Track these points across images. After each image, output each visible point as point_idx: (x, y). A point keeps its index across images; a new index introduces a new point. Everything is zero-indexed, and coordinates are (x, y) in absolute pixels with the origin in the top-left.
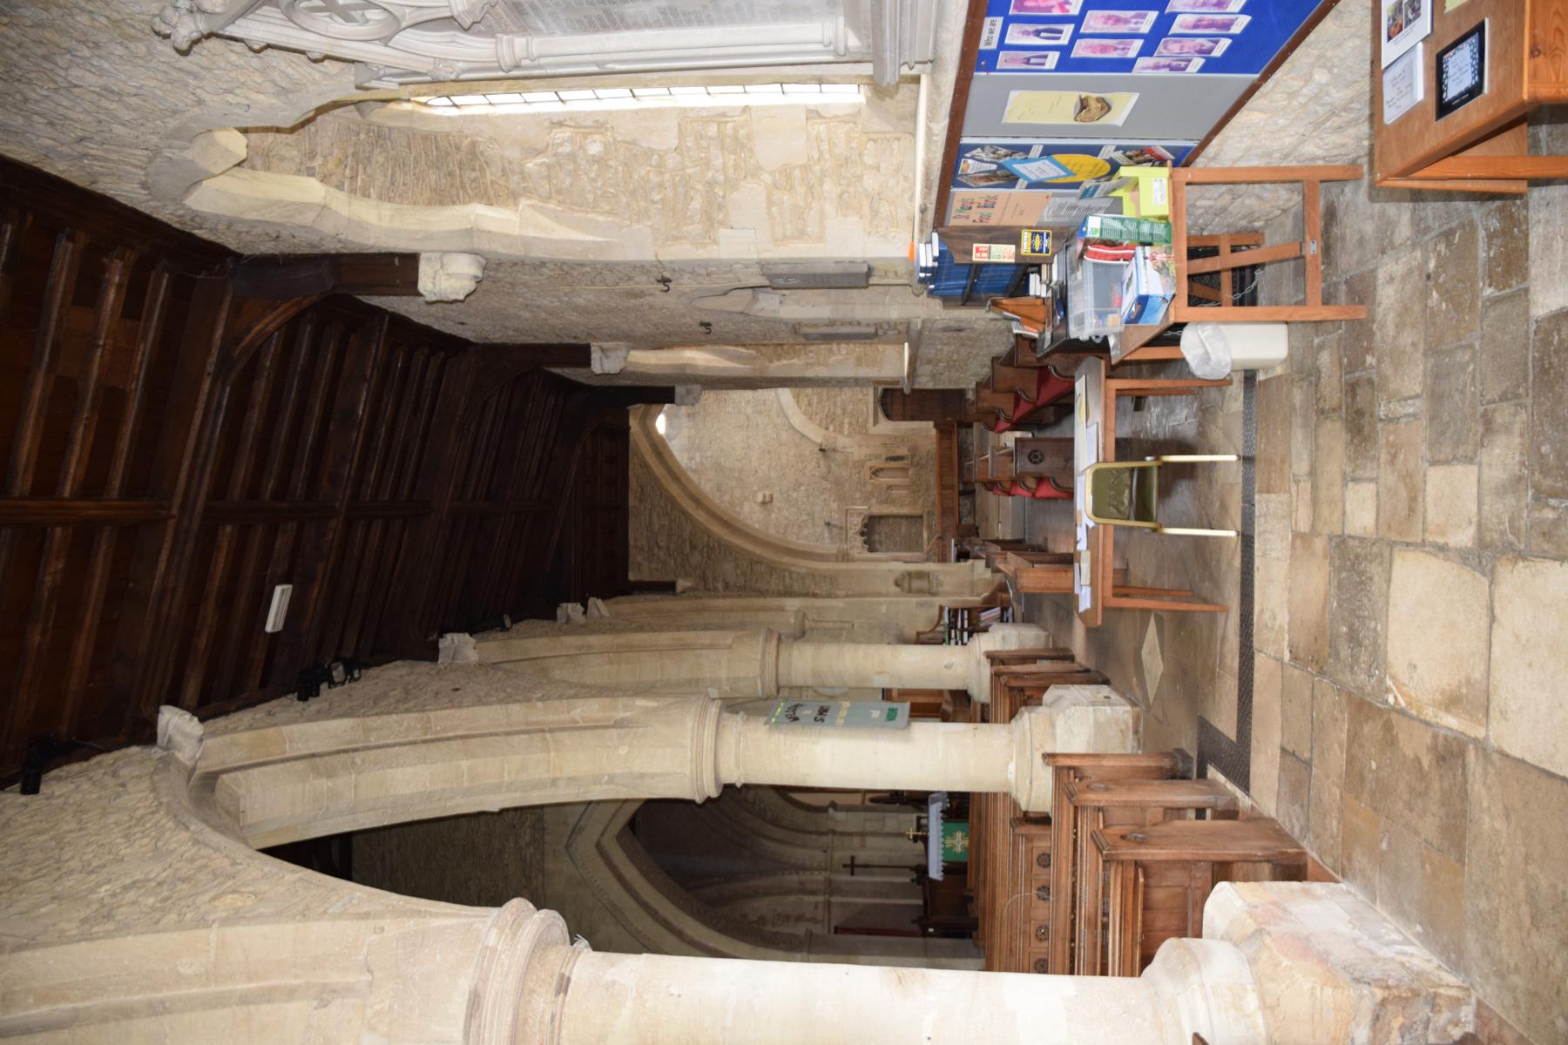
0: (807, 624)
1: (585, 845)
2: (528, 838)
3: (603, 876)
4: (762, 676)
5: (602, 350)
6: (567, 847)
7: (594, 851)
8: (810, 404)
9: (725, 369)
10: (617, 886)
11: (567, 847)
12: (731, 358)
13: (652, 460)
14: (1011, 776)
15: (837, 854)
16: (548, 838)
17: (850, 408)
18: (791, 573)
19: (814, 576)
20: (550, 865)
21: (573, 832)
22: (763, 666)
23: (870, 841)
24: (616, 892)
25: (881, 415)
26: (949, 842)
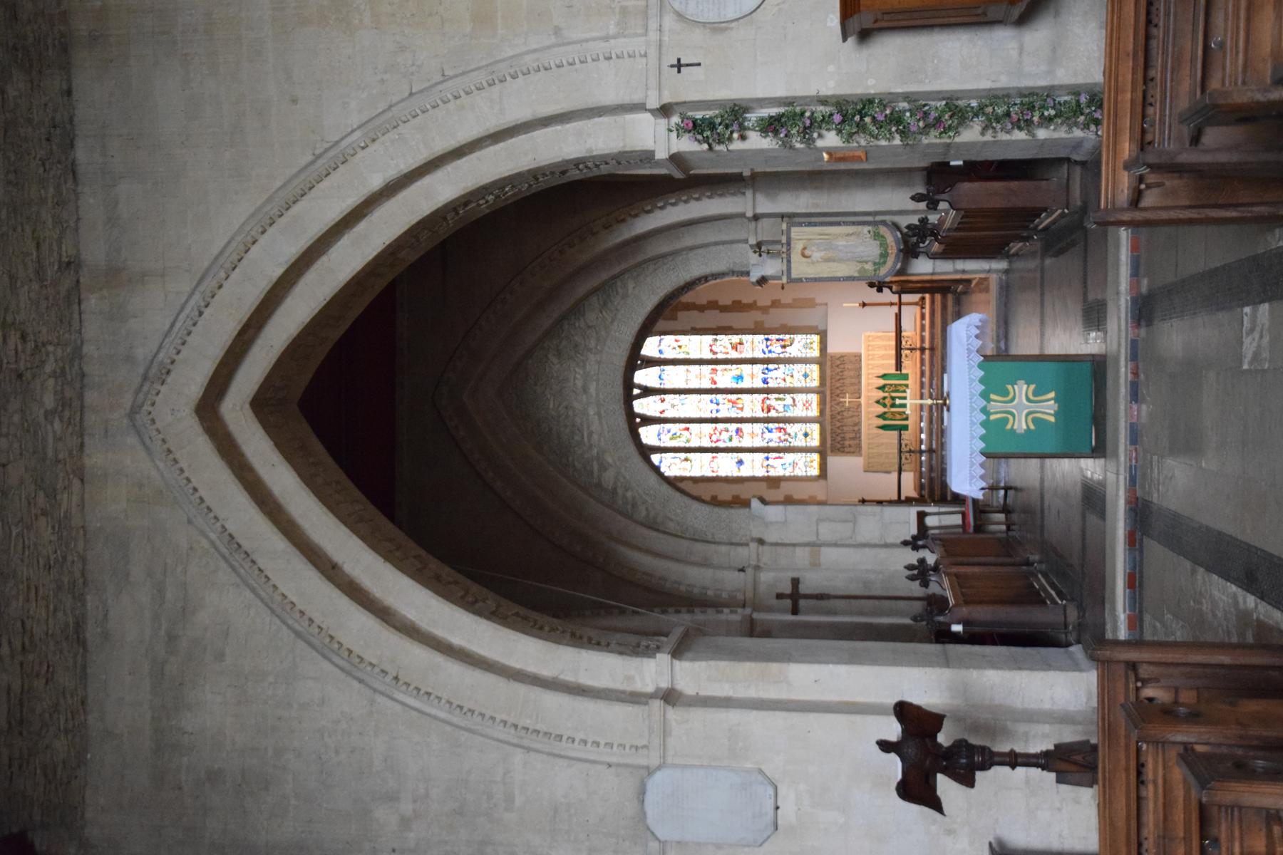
2: (49, 401)
6: (134, 411)
11: (134, 411)
20: (95, 458)
23: (829, 555)
26: (997, 404)
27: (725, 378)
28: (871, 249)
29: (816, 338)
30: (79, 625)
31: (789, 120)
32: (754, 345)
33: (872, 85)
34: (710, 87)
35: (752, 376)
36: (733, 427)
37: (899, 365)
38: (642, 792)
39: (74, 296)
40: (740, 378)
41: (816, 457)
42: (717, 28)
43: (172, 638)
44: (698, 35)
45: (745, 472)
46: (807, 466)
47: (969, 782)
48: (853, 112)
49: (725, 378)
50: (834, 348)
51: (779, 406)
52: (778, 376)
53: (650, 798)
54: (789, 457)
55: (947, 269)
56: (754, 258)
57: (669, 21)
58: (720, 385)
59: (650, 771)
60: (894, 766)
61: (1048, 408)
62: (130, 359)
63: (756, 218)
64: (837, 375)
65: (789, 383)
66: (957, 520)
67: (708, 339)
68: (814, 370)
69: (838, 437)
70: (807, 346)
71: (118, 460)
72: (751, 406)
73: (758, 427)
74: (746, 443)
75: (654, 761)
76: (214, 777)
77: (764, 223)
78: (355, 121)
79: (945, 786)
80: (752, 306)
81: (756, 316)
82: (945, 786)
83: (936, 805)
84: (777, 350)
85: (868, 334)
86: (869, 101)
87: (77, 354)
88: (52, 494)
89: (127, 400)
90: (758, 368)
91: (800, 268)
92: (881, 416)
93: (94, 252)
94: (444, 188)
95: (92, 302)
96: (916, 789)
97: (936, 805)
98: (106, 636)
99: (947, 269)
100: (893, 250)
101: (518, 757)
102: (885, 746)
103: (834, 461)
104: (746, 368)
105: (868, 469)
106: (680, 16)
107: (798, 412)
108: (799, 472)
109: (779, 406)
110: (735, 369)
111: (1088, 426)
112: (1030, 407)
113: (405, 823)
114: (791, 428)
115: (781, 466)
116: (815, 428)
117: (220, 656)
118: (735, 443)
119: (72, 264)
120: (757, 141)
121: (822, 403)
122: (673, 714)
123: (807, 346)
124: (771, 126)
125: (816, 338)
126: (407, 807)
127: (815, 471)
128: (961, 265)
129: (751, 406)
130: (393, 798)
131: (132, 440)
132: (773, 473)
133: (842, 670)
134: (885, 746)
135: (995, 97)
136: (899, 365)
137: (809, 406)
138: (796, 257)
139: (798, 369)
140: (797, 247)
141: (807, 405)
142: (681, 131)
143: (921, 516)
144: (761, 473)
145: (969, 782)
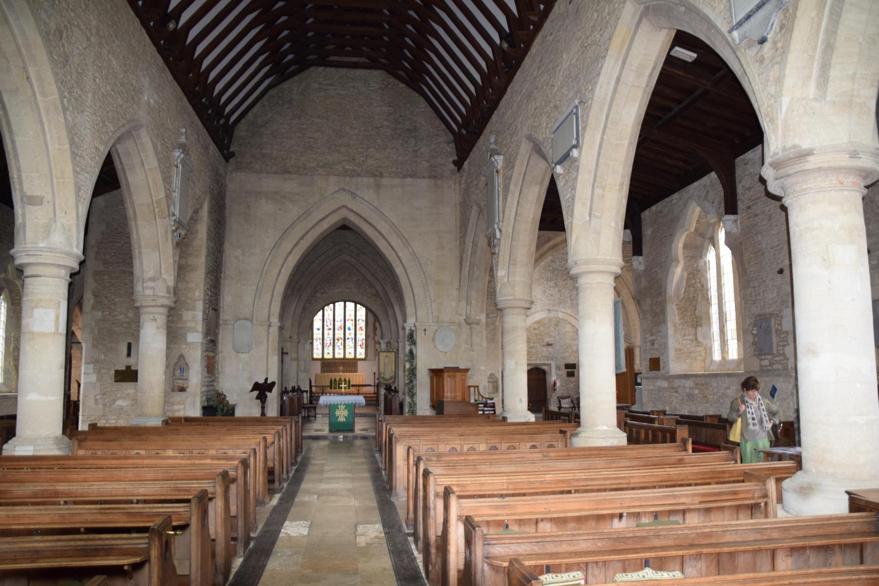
0: (473, 326)
1: (345, 199)
2: (347, 167)
3: (327, 208)
4: (515, 299)
5: (736, 221)
6: (344, 190)
7: (341, 204)
8: (535, 329)
9: (672, 282)
10: (321, 216)
11: (344, 190)
12: (678, 288)
13: (551, 243)
14: (600, 428)
15: (288, 344)
16: (348, 178)
17: (534, 351)
18: (496, 317)
19: (494, 329)
20: (332, 179)
21: (352, 193)
22: (519, 300)
23: (295, 363)
24: (316, 216)
25: (530, 367)
26: (343, 407)
27: (350, 324)
28: (387, 376)
29: (363, 357)
30: (289, 173)
31: (412, 355)
32: (361, 335)
33: (419, 376)
34: (419, 337)
35: (350, 334)
36: (332, 327)
37: (353, 386)
38: (246, 319)
39: (374, 176)
40: (349, 329)
41: (320, 357)
42: (433, 339)
43: (285, 197)
44: (432, 335)
45: (315, 331)
46: (317, 354)
47: (257, 398)
48: (413, 372)
49: (350, 324)
50: (359, 362)
51: (339, 344)
52: (350, 343)
53: (245, 322)
54: (320, 347)
55: (382, 398)
56: (386, 341)
57: (435, 328)
58: (347, 323)
59: (251, 321)
60: (261, 381)
61: (342, 419)
62: (357, 189)
63: (398, 342)
64: (350, 364)
65: (347, 347)
66: (305, 402)
67: (364, 318)
68: (352, 356)
69: (328, 365)
70: (361, 354)
71: (332, 184)
72: (339, 334)
73: (331, 336)
74: (326, 332)
75: (254, 322)
76: (249, 207)
77: (396, 345)
78: (415, 250)
79: (256, 393)
80: (375, 334)
81: (372, 335)
82: (256, 393)
83: (252, 391)
84: (359, 343)
85: (364, 375)
86: (415, 375)
87: (359, 175)
88: (323, 167)
89: (347, 188)
90: (353, 336)
91: (382, 355)
92: (335, 380)
93: (385, 181)
94: (399, 270)
95: (372, 180)
96: (256, 387)
97: (252, 391)
98: (286, 179)
99: (382, 398)
100: (387, 382)
101: (254, 288)
102: (266, 380)
103: (319, 363)
104: (353, 332)
105: (316, 375)
106: (436, 331)
107: (337, 351)
108: (315, 351)
109: (339, 344)
110: (353, 328)
111: (335, 427)
112: (342, 415)
113: (237, 258)
114: (331, 348)
115: (317, 345)
116: (331, 356)
117: (280, 210)
118: (326, 327)
119: (381, 176)
120: (408, 348)
121: (340, 359)
122: (266, 327)
123: (361, 354)
124: (411, 352)
125: (363, 357)
126: (241, 258)
127: (315, 356)
128: (383, 402)
129: (339, 334)
130: (243, 254)
131: (337, 189)
132: (315, 341)
133: (276, 369)
134: (266, 380)
135: (415, 404)
136: (353, 386)
137: (339, 355)
138: (386, 354)
139: (352, 350)
140: (389, 354)
141: (339, 354)
142: (411, 330)
143: (307, 392)
144: (315, 337)
145: (257, 398)
